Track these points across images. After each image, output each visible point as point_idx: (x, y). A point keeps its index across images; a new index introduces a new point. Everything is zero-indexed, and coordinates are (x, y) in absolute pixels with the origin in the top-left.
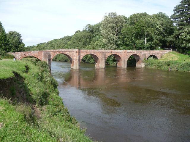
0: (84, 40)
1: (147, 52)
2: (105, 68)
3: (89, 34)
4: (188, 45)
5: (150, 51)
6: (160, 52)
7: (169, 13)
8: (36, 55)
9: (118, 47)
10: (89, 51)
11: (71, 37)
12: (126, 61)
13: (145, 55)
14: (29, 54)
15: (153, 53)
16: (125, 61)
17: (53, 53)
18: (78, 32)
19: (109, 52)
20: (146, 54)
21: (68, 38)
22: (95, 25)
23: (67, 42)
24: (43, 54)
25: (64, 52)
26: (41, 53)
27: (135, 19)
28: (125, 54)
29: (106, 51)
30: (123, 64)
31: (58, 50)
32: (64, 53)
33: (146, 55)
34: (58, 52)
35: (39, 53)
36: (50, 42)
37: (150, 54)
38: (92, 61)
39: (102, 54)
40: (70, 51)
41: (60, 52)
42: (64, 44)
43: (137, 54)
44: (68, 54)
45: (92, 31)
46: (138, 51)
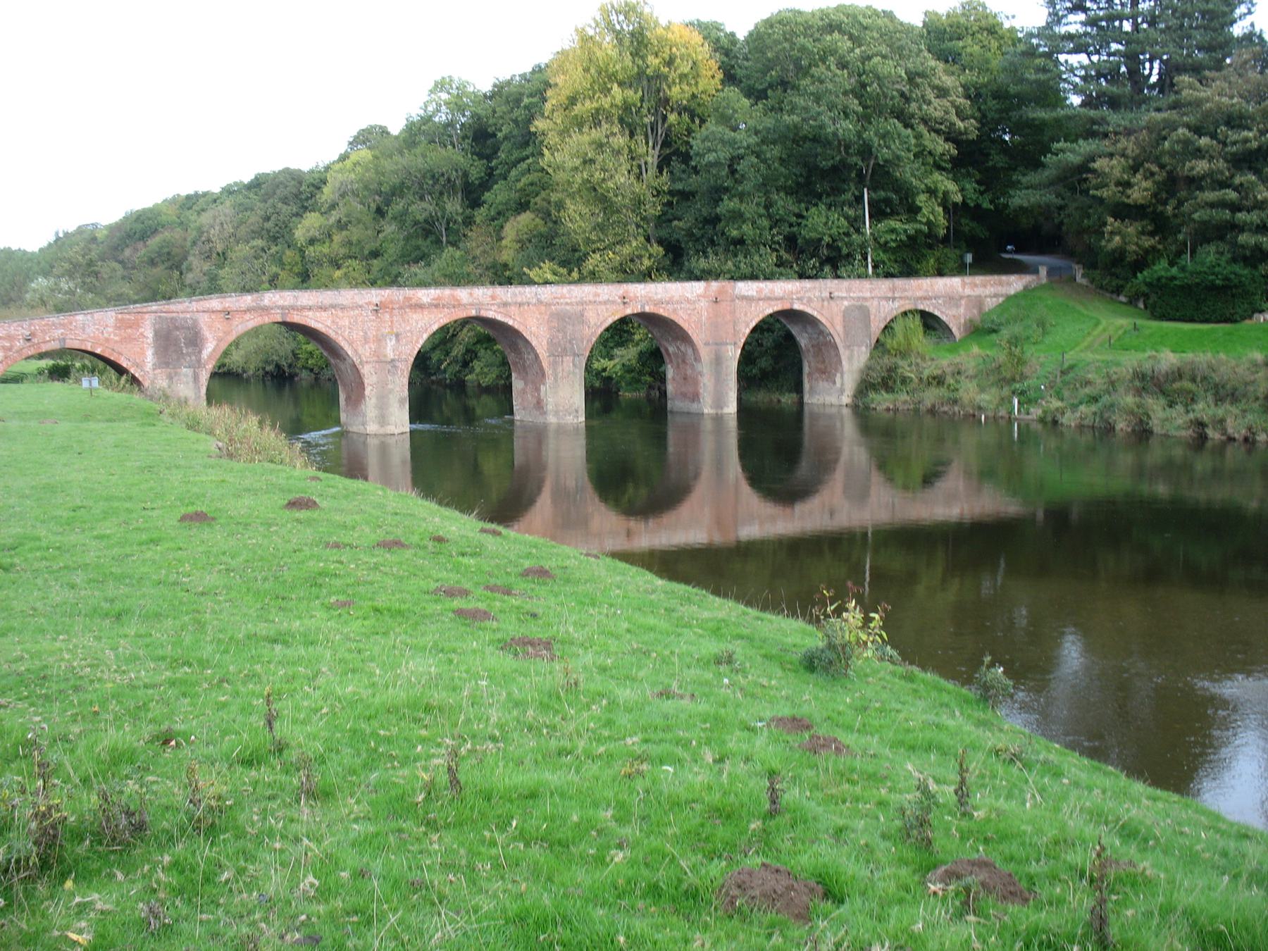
0: (421, 209)
1: (877, 293)
2: (589, 429)
3: (454, 158)
4: (1267, 241)
5: (899, 282)
6: (968, 291)
7: (741, 35)
8: (107, 340)
9: (675, 263)
10: (463, 294)
11: (317, 182)
12: (733, 355)
13: (864, 313)
14: (58, 333)
15: (919, 294)
16: (718, 361)
17: (220, 325)
18: (369, 137)
19: (603, 302)
20: (872, 306)
21: (297, 191)
22: (499, 91)
23: (279, 224)
24: (148, 331)
25: (293, 308)
26: (136, 325)
27: (765, 65)
28: (714, 313)
29: (586, 291)
30: (712, 392)
31: (248, 299)
32: (296, 318)
33: (873, 311)
34: (248, 316)
35: (121, 325)
36: (140, 227)
37: (895, 308)
38: (481, 373)
39: (558, 318)
40: (333, 306)
41: (266, 309)
42: (256, 234)
43: (809, 310)
44: (313, 324)
45: (481, 137)
46: (807, 284)
